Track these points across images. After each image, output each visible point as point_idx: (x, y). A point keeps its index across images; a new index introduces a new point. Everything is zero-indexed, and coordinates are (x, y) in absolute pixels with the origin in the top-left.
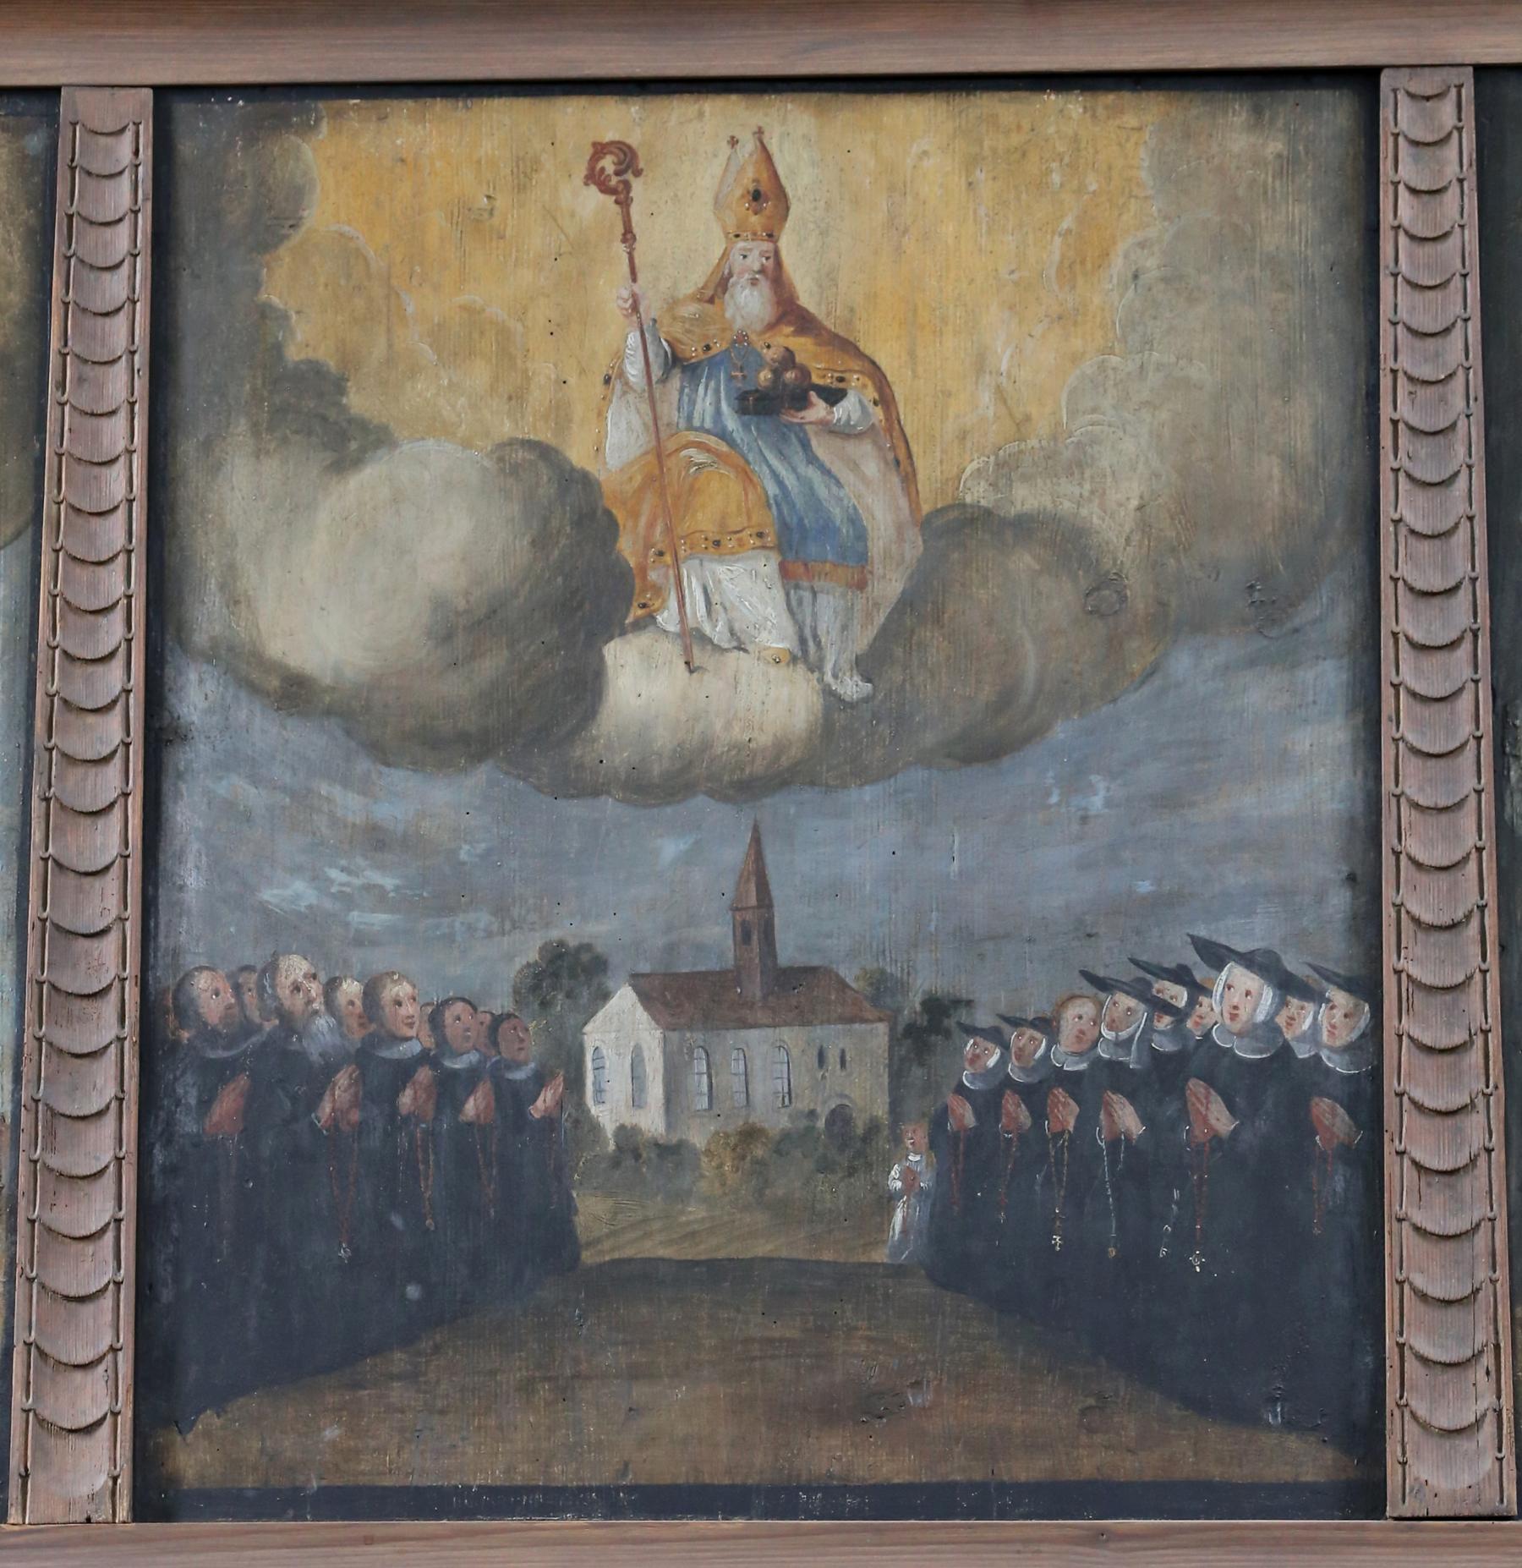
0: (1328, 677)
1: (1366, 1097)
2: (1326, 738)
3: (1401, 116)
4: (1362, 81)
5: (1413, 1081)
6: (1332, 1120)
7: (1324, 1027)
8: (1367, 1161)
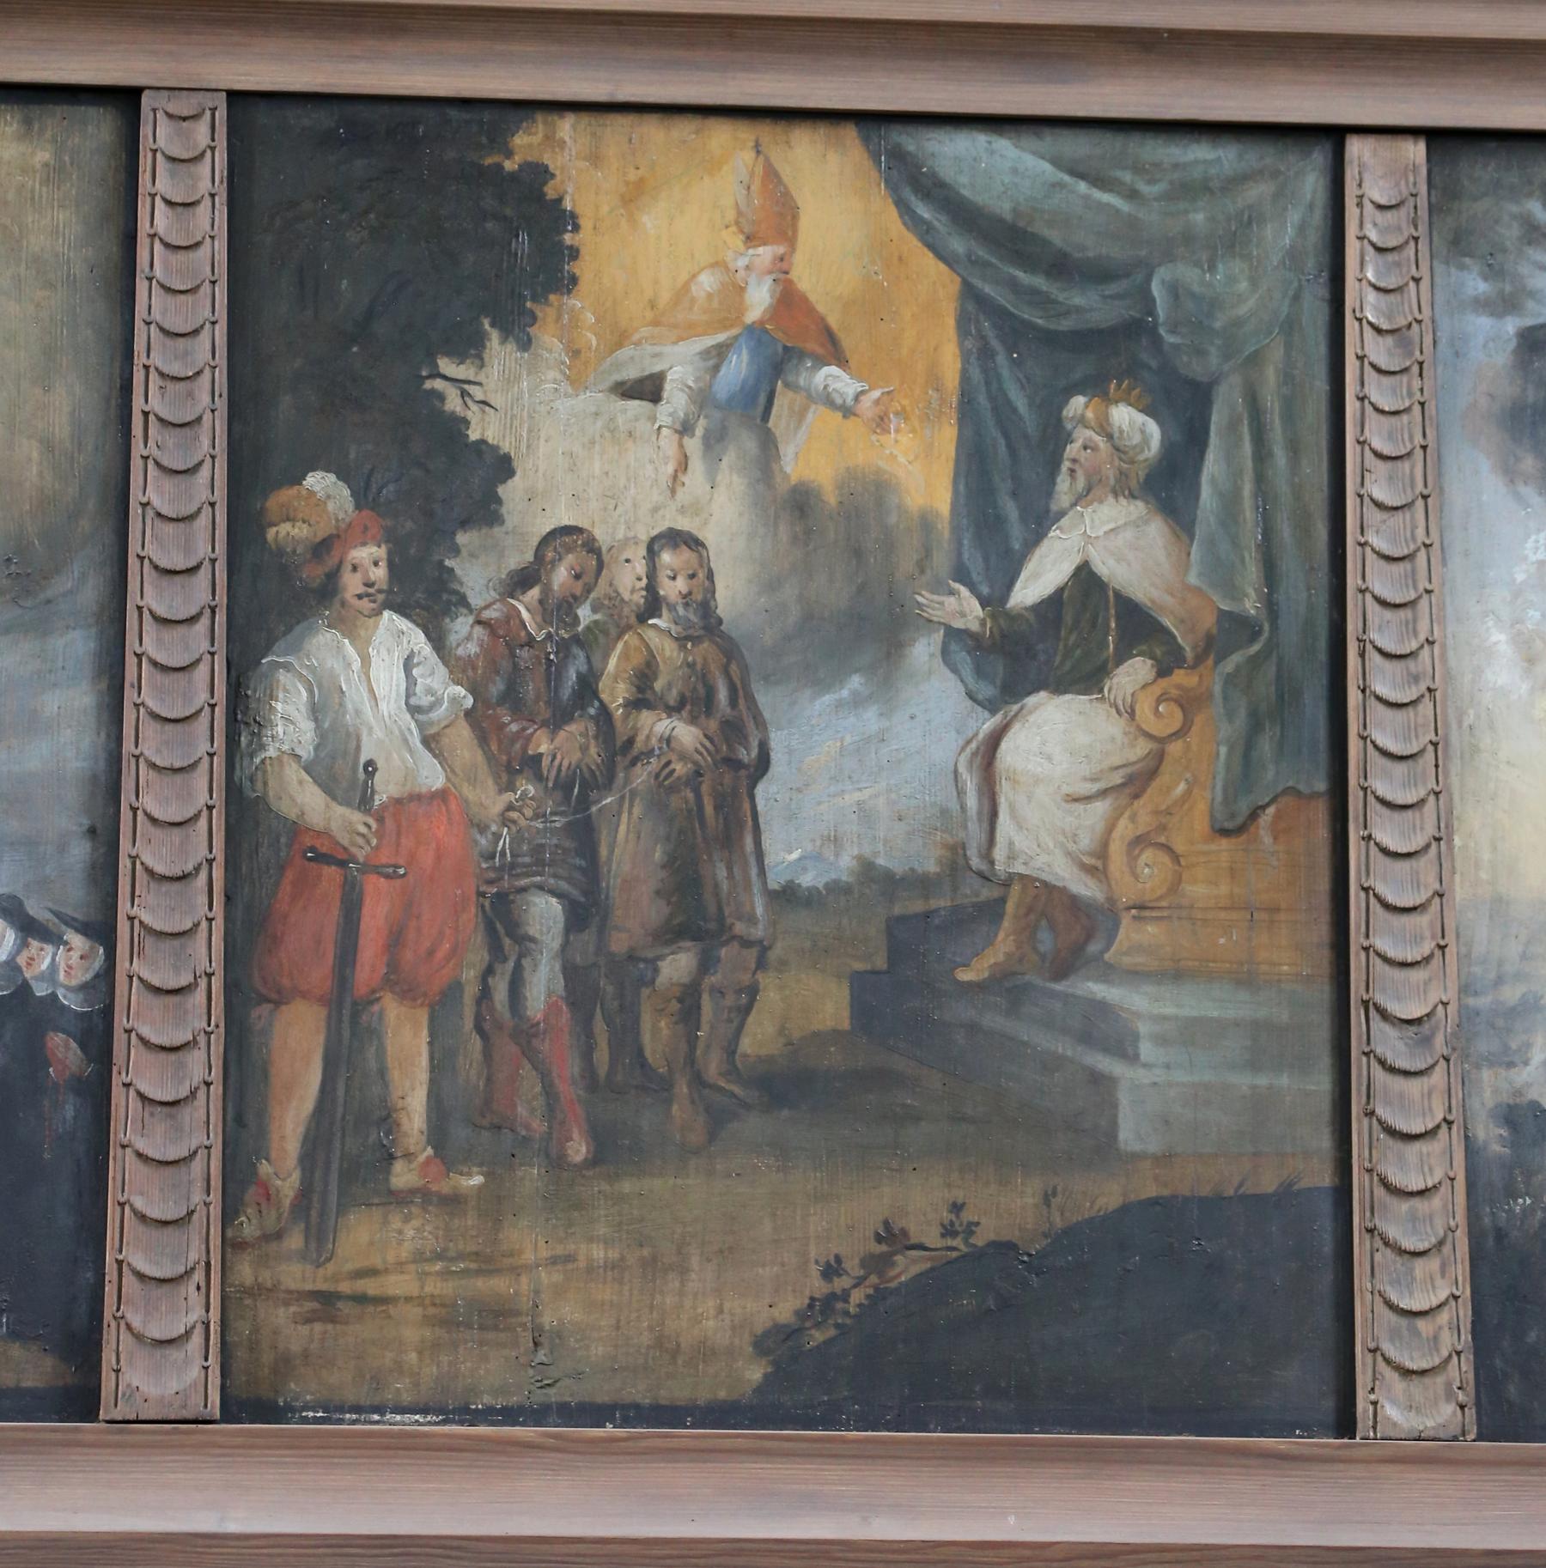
0: (76, 645)
1: (98, 1033)
2: (73, 702)
3: (159, 134)
4: (1336, 135)
5: (141, 1018)
6: (64, 1051)
7: (61, 967)
8: (96, 1092)
